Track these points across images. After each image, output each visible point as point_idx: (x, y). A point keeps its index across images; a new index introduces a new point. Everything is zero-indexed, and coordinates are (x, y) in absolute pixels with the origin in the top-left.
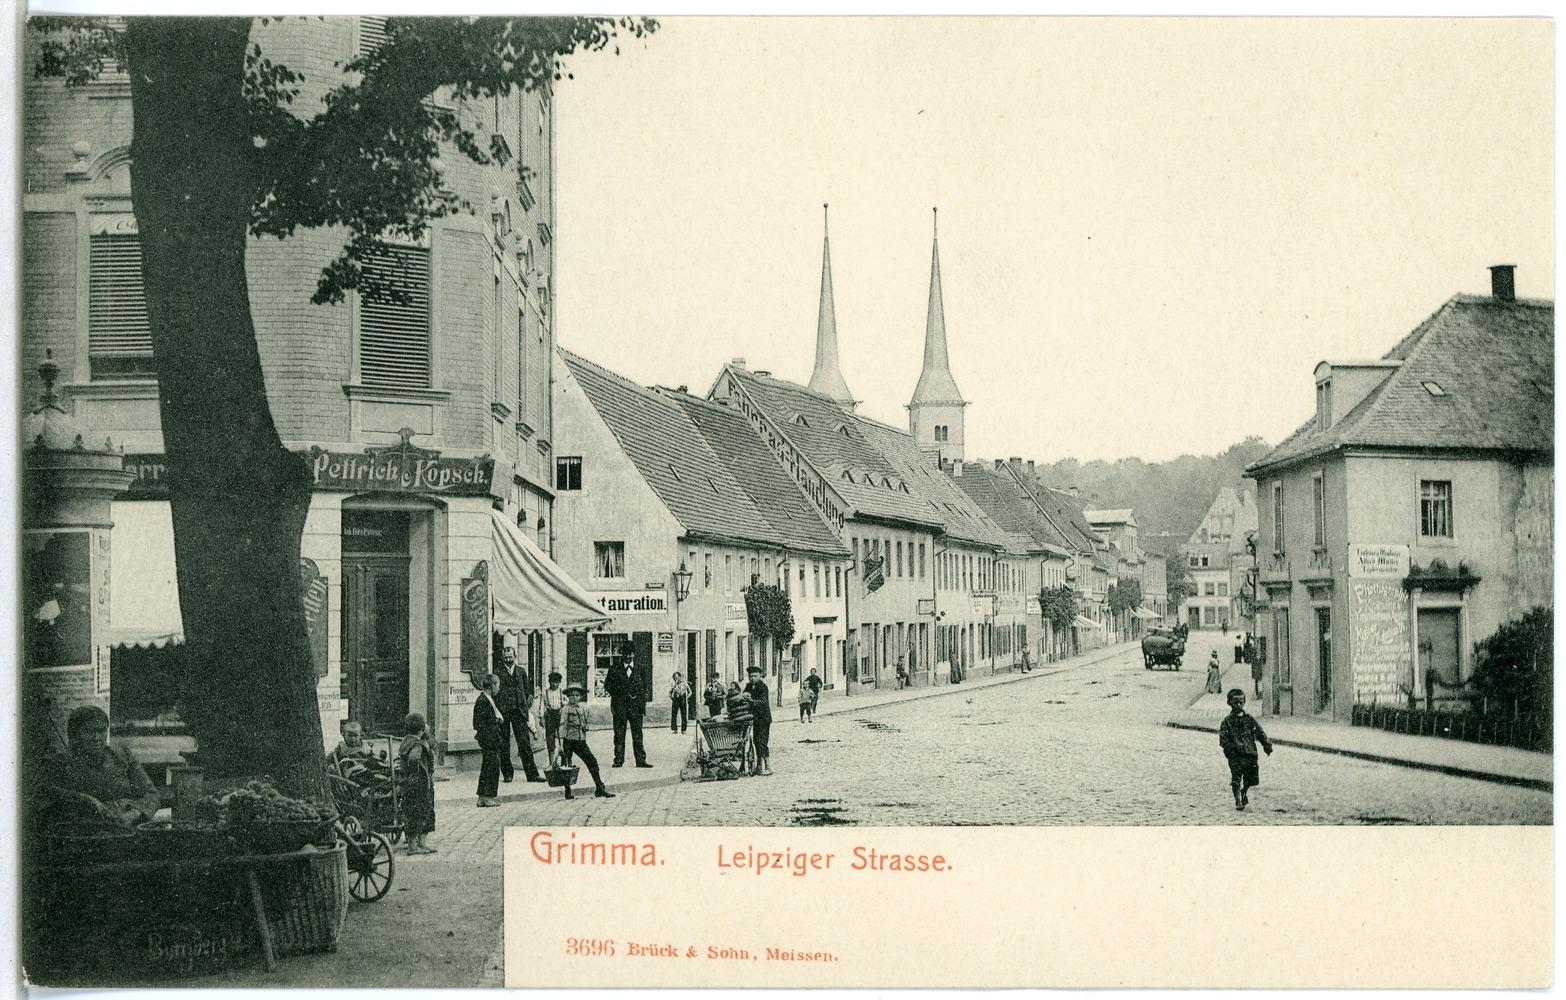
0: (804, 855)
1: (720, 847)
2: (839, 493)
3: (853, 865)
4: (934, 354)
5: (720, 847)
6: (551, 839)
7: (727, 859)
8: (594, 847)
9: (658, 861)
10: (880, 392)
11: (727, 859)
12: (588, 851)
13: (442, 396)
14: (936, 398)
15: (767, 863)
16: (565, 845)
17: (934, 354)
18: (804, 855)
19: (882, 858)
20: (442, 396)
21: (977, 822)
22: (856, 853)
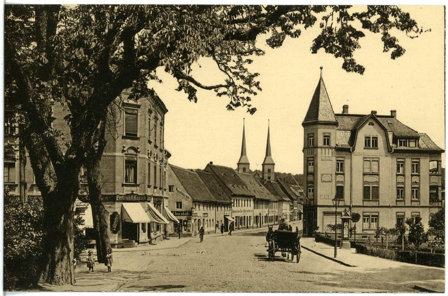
4: (268, 152)
14: (268, 164)
17: (268, 152)
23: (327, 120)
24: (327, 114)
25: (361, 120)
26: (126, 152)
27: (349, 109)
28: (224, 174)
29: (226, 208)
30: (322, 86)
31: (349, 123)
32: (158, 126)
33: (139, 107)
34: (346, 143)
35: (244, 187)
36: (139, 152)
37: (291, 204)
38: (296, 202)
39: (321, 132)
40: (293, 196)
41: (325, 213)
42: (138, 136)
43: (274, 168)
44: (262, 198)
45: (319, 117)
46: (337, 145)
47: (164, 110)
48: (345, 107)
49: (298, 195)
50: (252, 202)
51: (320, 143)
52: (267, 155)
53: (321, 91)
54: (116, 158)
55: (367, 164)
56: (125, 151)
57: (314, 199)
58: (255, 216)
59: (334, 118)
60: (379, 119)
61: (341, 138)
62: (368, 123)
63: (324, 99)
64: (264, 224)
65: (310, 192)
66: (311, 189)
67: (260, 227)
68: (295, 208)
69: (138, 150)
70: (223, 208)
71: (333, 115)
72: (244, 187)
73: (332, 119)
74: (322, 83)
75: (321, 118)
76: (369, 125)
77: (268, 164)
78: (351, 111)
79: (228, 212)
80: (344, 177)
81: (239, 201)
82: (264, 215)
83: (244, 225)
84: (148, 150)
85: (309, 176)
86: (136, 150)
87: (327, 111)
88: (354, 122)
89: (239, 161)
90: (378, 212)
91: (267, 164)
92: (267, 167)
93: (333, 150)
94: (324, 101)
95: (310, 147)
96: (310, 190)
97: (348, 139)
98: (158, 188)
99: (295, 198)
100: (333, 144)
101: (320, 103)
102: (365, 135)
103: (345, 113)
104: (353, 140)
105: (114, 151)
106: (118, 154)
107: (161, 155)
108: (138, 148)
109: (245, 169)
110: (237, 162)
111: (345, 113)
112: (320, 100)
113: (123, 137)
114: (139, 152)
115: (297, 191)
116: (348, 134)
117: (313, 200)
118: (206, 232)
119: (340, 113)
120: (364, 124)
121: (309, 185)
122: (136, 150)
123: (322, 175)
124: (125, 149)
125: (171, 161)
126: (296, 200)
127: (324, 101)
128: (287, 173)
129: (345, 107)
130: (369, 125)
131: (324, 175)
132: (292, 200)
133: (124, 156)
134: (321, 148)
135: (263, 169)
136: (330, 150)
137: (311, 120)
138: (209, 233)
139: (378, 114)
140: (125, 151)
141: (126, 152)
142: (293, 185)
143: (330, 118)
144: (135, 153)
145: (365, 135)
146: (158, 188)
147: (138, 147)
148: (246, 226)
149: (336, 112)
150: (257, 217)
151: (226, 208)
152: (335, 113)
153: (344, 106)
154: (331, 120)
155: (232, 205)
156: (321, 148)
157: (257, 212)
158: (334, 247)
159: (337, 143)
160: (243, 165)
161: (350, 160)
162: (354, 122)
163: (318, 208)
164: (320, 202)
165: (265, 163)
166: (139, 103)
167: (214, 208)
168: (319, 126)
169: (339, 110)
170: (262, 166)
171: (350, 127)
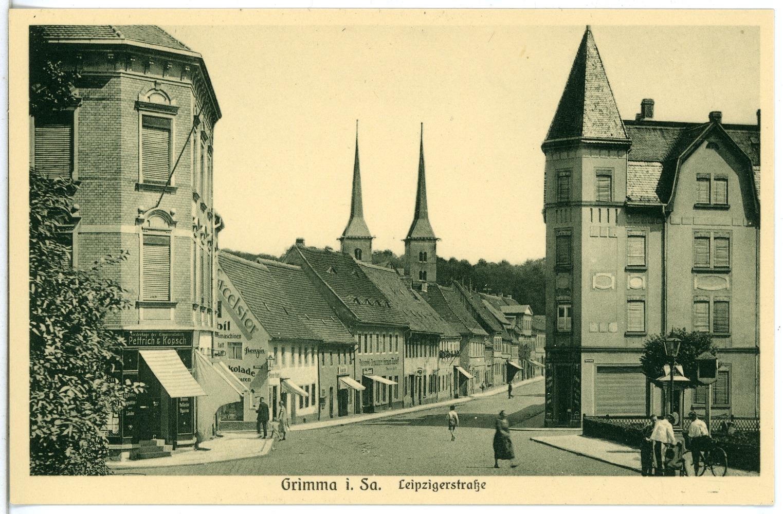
0: (437, 483)
1: (600, 221)
2: (272, 503)
3: (361, 488)
4: (420, 211)
5: (600, 221)
6: (289, 481)
7: (403, 485)
8: (309, 483)
9: (378, 488)
10: (388, 233)
11: (403, 485)
12: (307, 485)
13: (242, 398)
14: (420, 236)
15: (371, 485)
16: (296, 483)
17: (420, 211)
18: (437, 483)
19: (463, 484)
20: (242, 398)
21: (575, 455)
22: (362, 481)
23: (604, 136)
25: (686, 137)
26: (145, 225)
29: (342, 355)
30: (591, 51)
31: (660, 144)
32: (206, 154)
34: (652, 194)
35: (383, 303)
36: (174, 223)
38: (497, 338)
39: (590, 164)
40: (491, 323)
46: (629, 199)
47: (214, 114)
48: (647, 106)
51: (589, 192)
52: (417, 216)
53: (589, 64)
54: (123, 238)
55: (702, 247)
56: (142, 221)
60: (730, 132)
62: (706, 143)
65: (562, 315)
68: (496, 354)
69: (174, 218)
70: (335, 356)
72: (383, 303)
73: (618, 134)
74: (589, 44)
75: (590, 130)
76: (708, 147)
77: (420, 236)
78: (659, 115)
79: (346, 367)
82: (429, 372)
84: (194, 218)
86: (168, 218)
87: (605, 112)
89: (344, 234)
91: (415, 240)
93: (619, 210)
94: (598, 89)
95: (561, 202)
97: (655, 183)
99: (496, 327)
100: (620, 198)
101: (587, 94)
102: (698, 174)
103: (644, 118)
104: (666, 187)
105: (118, 218)
107: (210, 225)
108: (172, 214)
110: (340, 235)
112: (587, 85)
114: (174, 223)
115: (500, 310)
116: (656, 170)
117: (572, 334)
120: (697, 146)
121: (561, 298)
122: (168, 218)
124: (142, 216)
127: (598, 89)
128: (459, 258)
129: (647, 106)
130: (708, 147)
132: (491, 332)
134: (590, 205)
135: (408, 251)
136: (612, 210)
137: (565, 133)
139: (725, 120)
140: (142, 221)
141: (145, 225)
144: (166, 226)
145: (698, 174)
146: (206, 311)
147: (174, 210)
148: (387, 402)
151: (342, 355)
155: (356, 347)
156: (590, 205)
158: (724, 468)
159: (629, 193)
160: (356, 239)
161: (659, 234)
162: (669, 141)
163: (584, 356)
164: (587, 341)
165: (414, 236)
167: (316, 356)
168: (583, 152)
169: (631, 111)
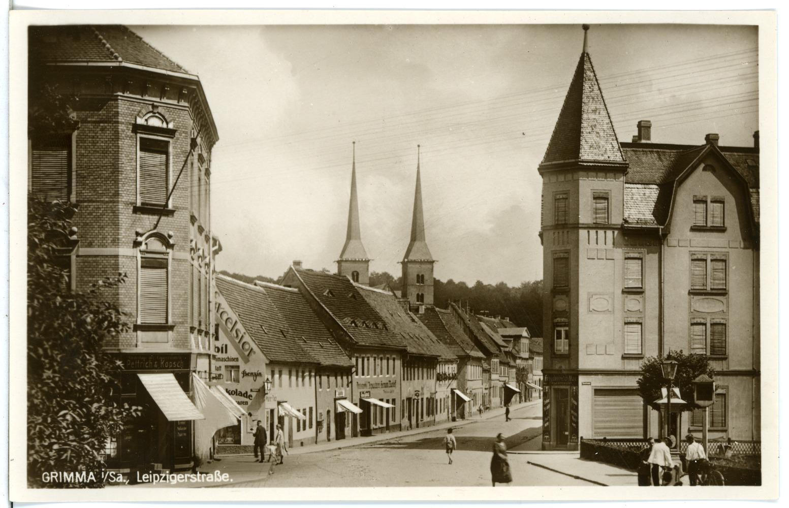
23: (601, 158)
24: (602, 143)
27: (652, 130)
28: (330, 292)
32: (203, 177)
33: (171, 133)
34: (649, 217)
35: (380, 325)
37: (485, 365)
38: (495, 360)
40: (488, 345)
41: (598, 392)
42: (170, 207)
43: (432, 270)
44: (422, 352)
45: (582, 151)
46: (626, 221)
48: (644, 128)
49: (500, 342)
50: (398, 363)
51: (585, 217)
54: (121, 260)
57: (572, 354)
58: (404, 397)
59: (619, 154)
60: (726, 154)
61: (638, 203)
62: (702, 165)
63: (592, 106)
64: (426, 419)
65: (559, 337)
66: (563, 330)
67: (417, 426)
68: (494, 377)
69: (171, 241)
70: (332, 379)
71: (616, 146)
73: (616, 157)
74: (587, 66)
75: (587, 154)
76: (704, 169)
78: (656, 138)
80: (644, 300)
81: (368, 360)
82: (427, 395)
83: (381, 423)
85: (558, 297)
88: (666, 163)
90: (727, 388)
92: (414, 270)
93: (616, 232)
96: (559, 333)
98: (196, 332)
99: (493, 349)
102: (695, 196)
106: (125, 250)
108: (170, 236)
109: (358, 274)
110: (338, 258)
111: (643, 141)
113: (136, 210)
116: (653, 192)
118: (297, 441)
119: (630, 140)
120: (694, 168)
122: (164, 240)
123: (590, 296)
124: (140, 239)
125: (220, 263)
126: (497, 356)
127: (594, 111)
129: (644, 128)
130: (704, 169)
131: (595, 297)
133: (139, 255)
134: (588, 227)
136: (609, 233)
138: (302, 444)
139: (721, 143)
142: (485, 318)
143: (609, 154)
147: (171, 233)
148: (384, 425)
149: (622, 139)
150: (409, 399)
152: (620, 140)
153: (640, 123)
154: (612, 159)
155: (354, 370)
157: (408, 388)
159: (626, 215)
163: (582, 379)
164: (585, 362)
166: (171, 126)
168: (581, 173)
169: (628, 134)
170: (400, 266)
171: (658, 175)
